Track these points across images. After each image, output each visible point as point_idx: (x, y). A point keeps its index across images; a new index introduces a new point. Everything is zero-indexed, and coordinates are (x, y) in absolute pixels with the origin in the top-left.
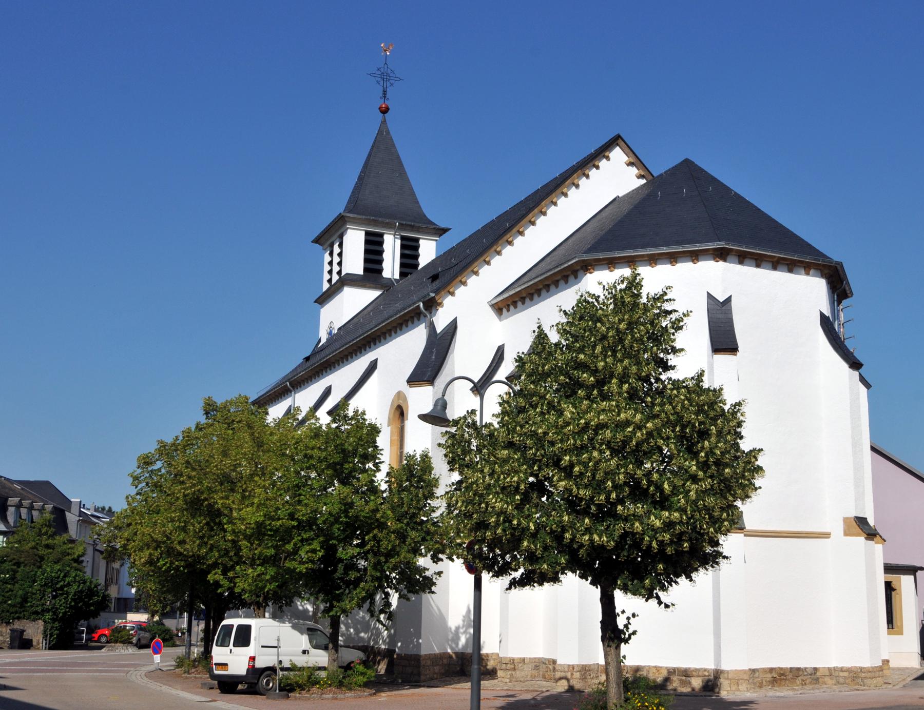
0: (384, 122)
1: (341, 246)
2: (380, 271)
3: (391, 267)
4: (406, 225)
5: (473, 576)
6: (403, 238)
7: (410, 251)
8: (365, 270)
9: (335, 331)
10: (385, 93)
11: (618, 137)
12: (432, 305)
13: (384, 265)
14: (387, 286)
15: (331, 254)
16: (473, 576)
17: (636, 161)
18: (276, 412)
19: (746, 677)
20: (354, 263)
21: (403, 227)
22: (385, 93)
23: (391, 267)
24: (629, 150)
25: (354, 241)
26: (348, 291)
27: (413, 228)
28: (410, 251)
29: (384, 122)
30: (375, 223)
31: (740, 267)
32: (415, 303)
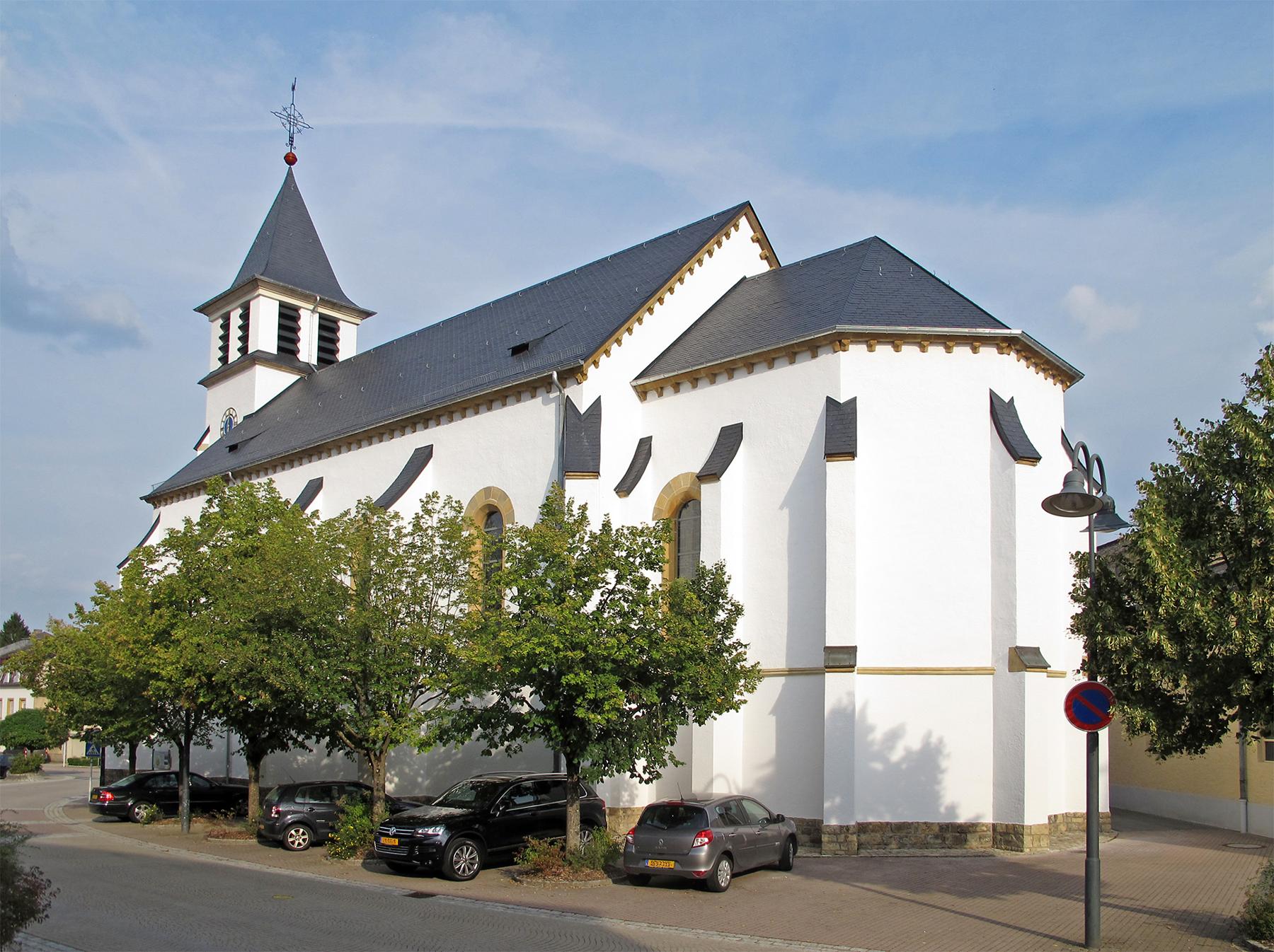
0: (290, 174)
1: (245, 316)
2: (294, 353)
3: (308, 350)
4: (328, 302)
5: (1084, 733)
6: (322, 317)
7: (328, 331)
8: (279, 349)
9: (240, 420)
10: (291, 139)
11: (748, 204)
12: (574, 373)
13: (301, 345)
14: (305, 369)
15: (226, 327)
16: (1084, 733)
17: (762, 239)
18: (407, 506)
19: (1047, 832)
20: (265, 337)
21: (324, 302)
22: (291, 139)
23: (308, 350)
24: (756, 225)
25: (265, 310)
26: (260, 371)
27: (333, 306)
28: (328, 331)
29: (290, 174)
30: (292, 293)
31: (714, 387)
32: (544, 368)
